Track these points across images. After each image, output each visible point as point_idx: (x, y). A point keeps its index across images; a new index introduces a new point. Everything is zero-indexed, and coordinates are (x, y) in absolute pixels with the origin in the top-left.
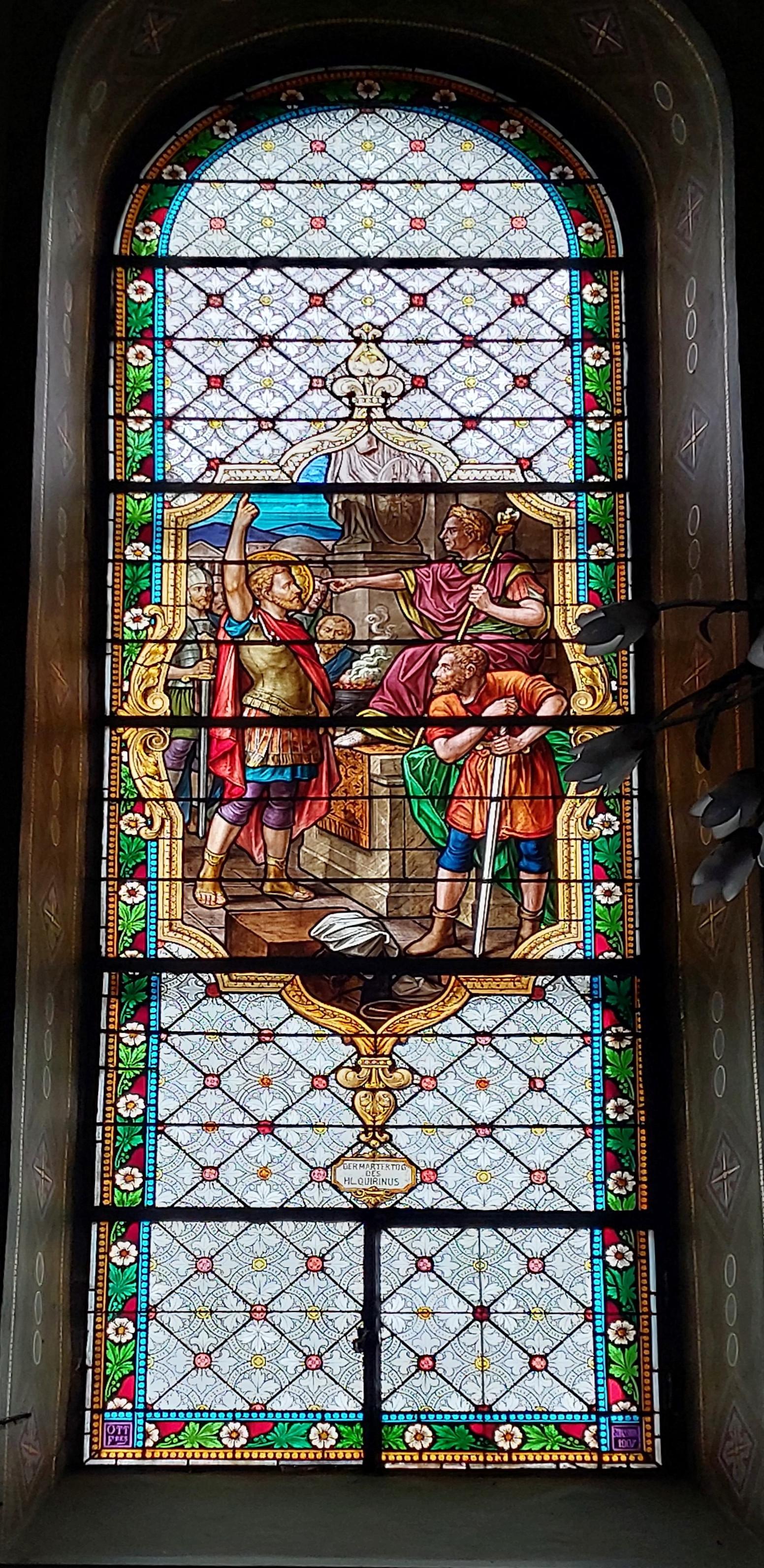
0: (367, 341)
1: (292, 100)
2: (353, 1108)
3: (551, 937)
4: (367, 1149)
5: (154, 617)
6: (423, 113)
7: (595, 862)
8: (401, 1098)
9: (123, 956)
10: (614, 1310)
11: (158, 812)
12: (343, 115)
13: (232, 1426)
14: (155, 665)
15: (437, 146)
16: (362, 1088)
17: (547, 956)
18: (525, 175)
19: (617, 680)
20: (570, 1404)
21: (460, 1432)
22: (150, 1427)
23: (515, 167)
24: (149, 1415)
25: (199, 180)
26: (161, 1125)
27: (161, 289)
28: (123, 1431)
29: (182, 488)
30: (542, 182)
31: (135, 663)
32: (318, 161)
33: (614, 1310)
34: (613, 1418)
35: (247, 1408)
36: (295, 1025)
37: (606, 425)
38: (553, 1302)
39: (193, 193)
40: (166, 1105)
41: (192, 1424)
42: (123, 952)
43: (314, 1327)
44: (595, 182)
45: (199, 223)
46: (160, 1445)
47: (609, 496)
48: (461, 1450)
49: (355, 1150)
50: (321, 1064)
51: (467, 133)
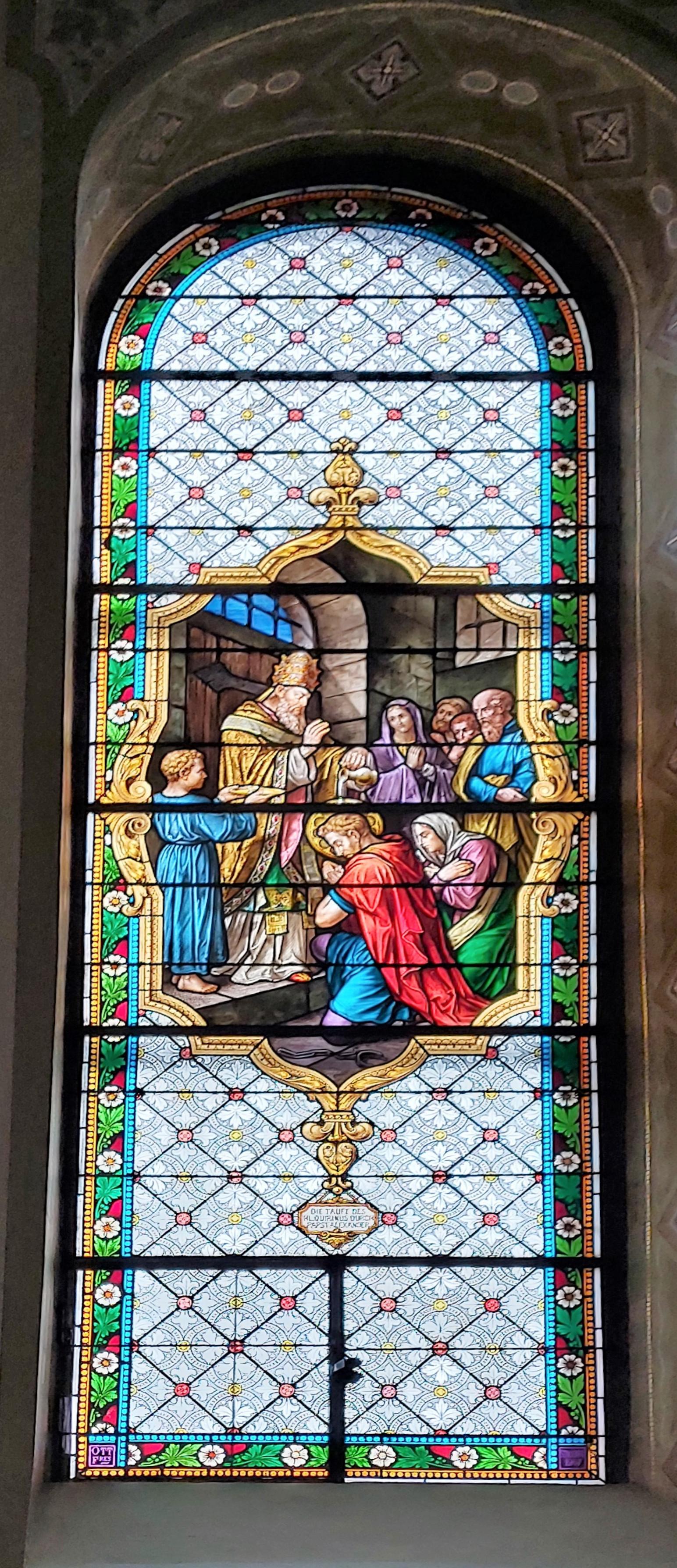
0: (345, 453)
1: (272, 219)
2: (317, 1159)
3: (511, 1005)
4: (331, 1196)
5: (136, 711)
6: (400, 231)
7: (541, 324)
8: (362, 1148)
9: (105, 1025)
10: (558, 450)
11: (140, 891)
12: (323, 233)
13: (209, 1448)
14: (137, 756)
15: (413, 262)
16: (326, 1141)
17: (506, 1024)
18: (500, 291)
19: (578, 770)
20: (521, 1428)
21: (421, 1451)
22: (132, 1448)
23: (489, 284)
24: (131, 1437)
25: (182, 296)
26: (135, 1177)
27: (147, 402)
28: (106, 1453)
29: (162, 590)
30: (515, 297)
31: (118, 755)
32: (297, 277)
33: (558, 450)
34: (561, 1440)
35: (223, 1431)
36: (263, 1084)
37: (572, 656)
38: (478, 1359)
39: (177, 310)
40: (141, 1158)
41: (172, 1446)
42: (106, 1021)
43: (288, 1359)
44: (566, 297)
45: (181, 338)
46: (142, 1465)
47: (572, 598)
48: (421, 1469)
49: (318, 1197)
50: (287, 1119)
51: (443, 251)
